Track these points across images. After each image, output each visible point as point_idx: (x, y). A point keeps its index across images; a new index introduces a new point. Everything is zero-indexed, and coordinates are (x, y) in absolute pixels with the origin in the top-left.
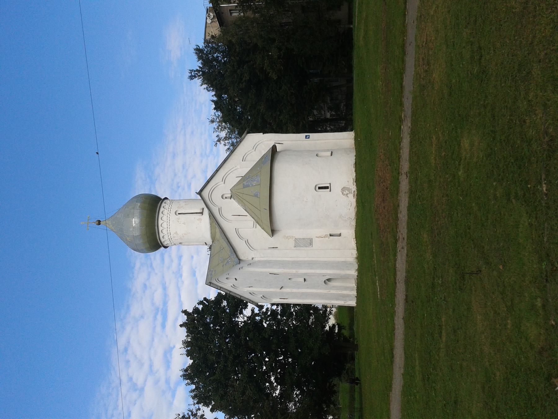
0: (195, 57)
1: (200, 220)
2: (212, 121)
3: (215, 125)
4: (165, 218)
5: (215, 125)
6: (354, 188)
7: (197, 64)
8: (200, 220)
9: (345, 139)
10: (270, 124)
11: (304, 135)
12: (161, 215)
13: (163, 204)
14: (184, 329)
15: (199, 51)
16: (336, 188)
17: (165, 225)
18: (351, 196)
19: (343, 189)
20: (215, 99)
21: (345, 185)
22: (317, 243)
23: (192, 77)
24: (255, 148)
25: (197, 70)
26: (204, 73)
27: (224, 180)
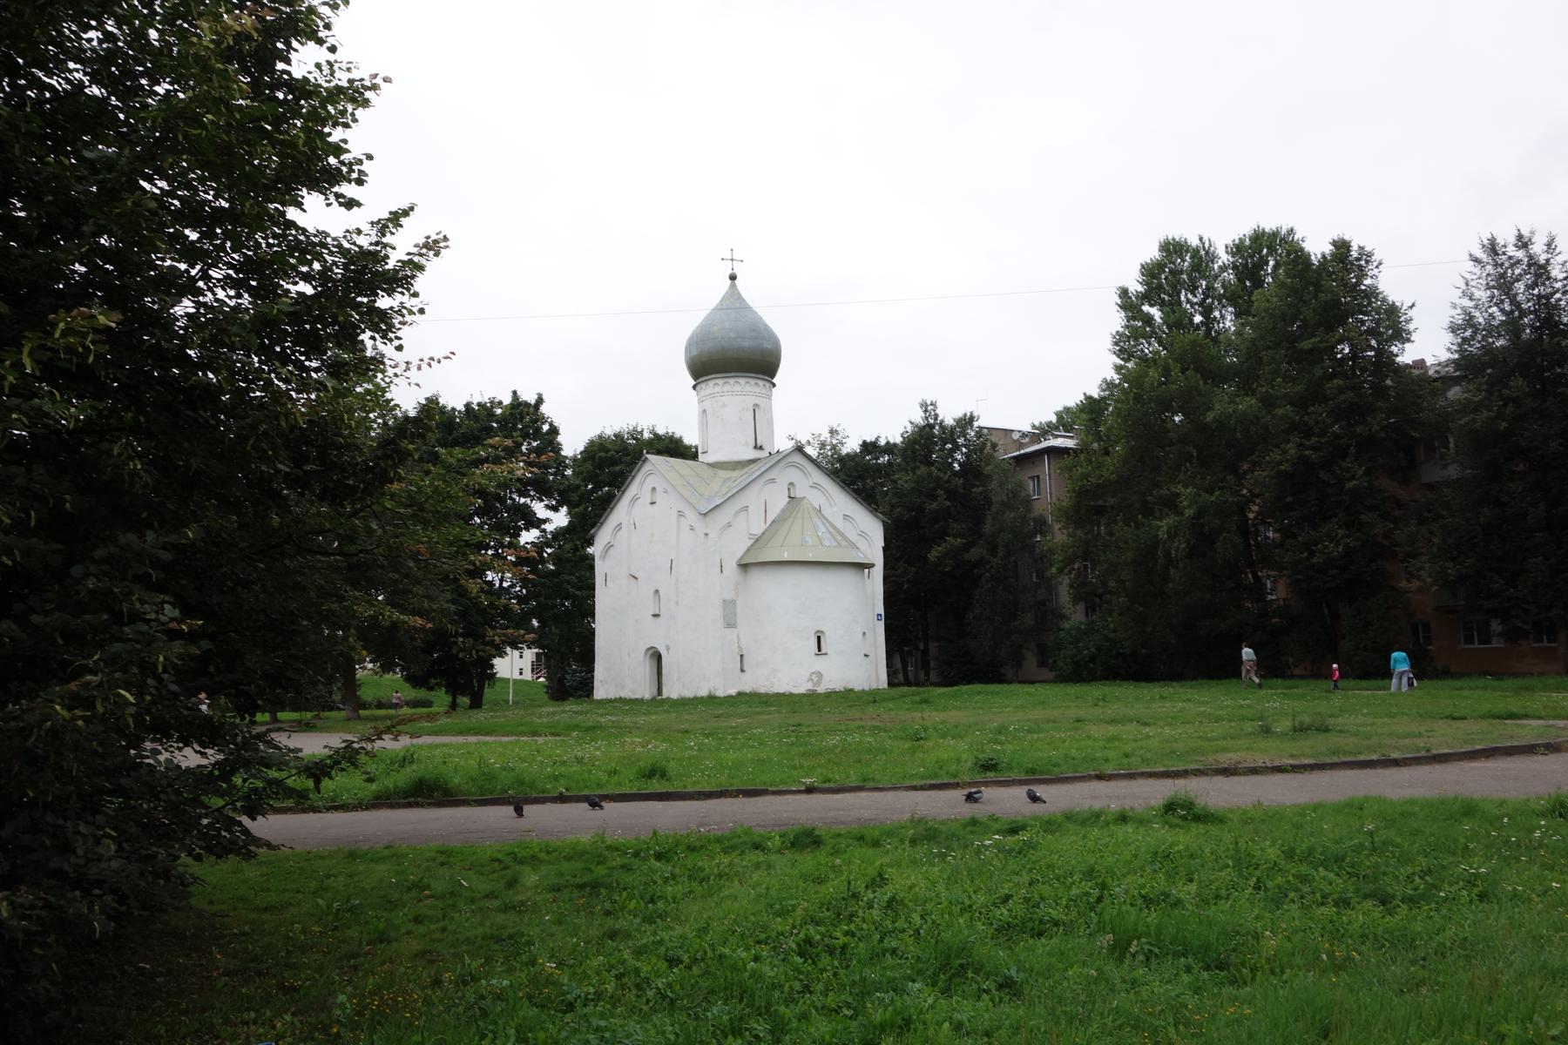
0: (959, 414)
1: (747, 444)
2: (833, 432)
3: (826, 436)
4: (748, 388)
5: (826, 436)
6: (821, 689)
7: (948, 415)
8: (747, 444)
9: (881, 680)
10: (401, 504)
11: (882, 612)
12: (753, 381)
13: (761, 383)
14: (532, 400)
15: (967, 422)
16: (820, 664)
17: (737, 388)
18: (810, 686)
19: (819, 674)
20: (882, 442)
21: (825, 677)
22: (731, 635)
23: (924, 406)
24: (863, 534)
25: (936, 416)
26: (931, 427)
27: (815, 486)
